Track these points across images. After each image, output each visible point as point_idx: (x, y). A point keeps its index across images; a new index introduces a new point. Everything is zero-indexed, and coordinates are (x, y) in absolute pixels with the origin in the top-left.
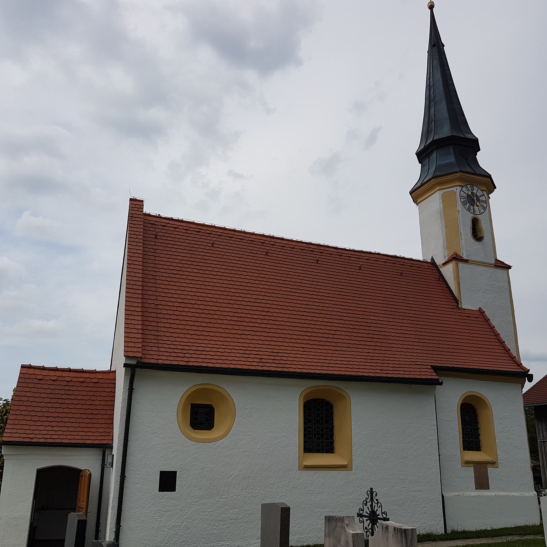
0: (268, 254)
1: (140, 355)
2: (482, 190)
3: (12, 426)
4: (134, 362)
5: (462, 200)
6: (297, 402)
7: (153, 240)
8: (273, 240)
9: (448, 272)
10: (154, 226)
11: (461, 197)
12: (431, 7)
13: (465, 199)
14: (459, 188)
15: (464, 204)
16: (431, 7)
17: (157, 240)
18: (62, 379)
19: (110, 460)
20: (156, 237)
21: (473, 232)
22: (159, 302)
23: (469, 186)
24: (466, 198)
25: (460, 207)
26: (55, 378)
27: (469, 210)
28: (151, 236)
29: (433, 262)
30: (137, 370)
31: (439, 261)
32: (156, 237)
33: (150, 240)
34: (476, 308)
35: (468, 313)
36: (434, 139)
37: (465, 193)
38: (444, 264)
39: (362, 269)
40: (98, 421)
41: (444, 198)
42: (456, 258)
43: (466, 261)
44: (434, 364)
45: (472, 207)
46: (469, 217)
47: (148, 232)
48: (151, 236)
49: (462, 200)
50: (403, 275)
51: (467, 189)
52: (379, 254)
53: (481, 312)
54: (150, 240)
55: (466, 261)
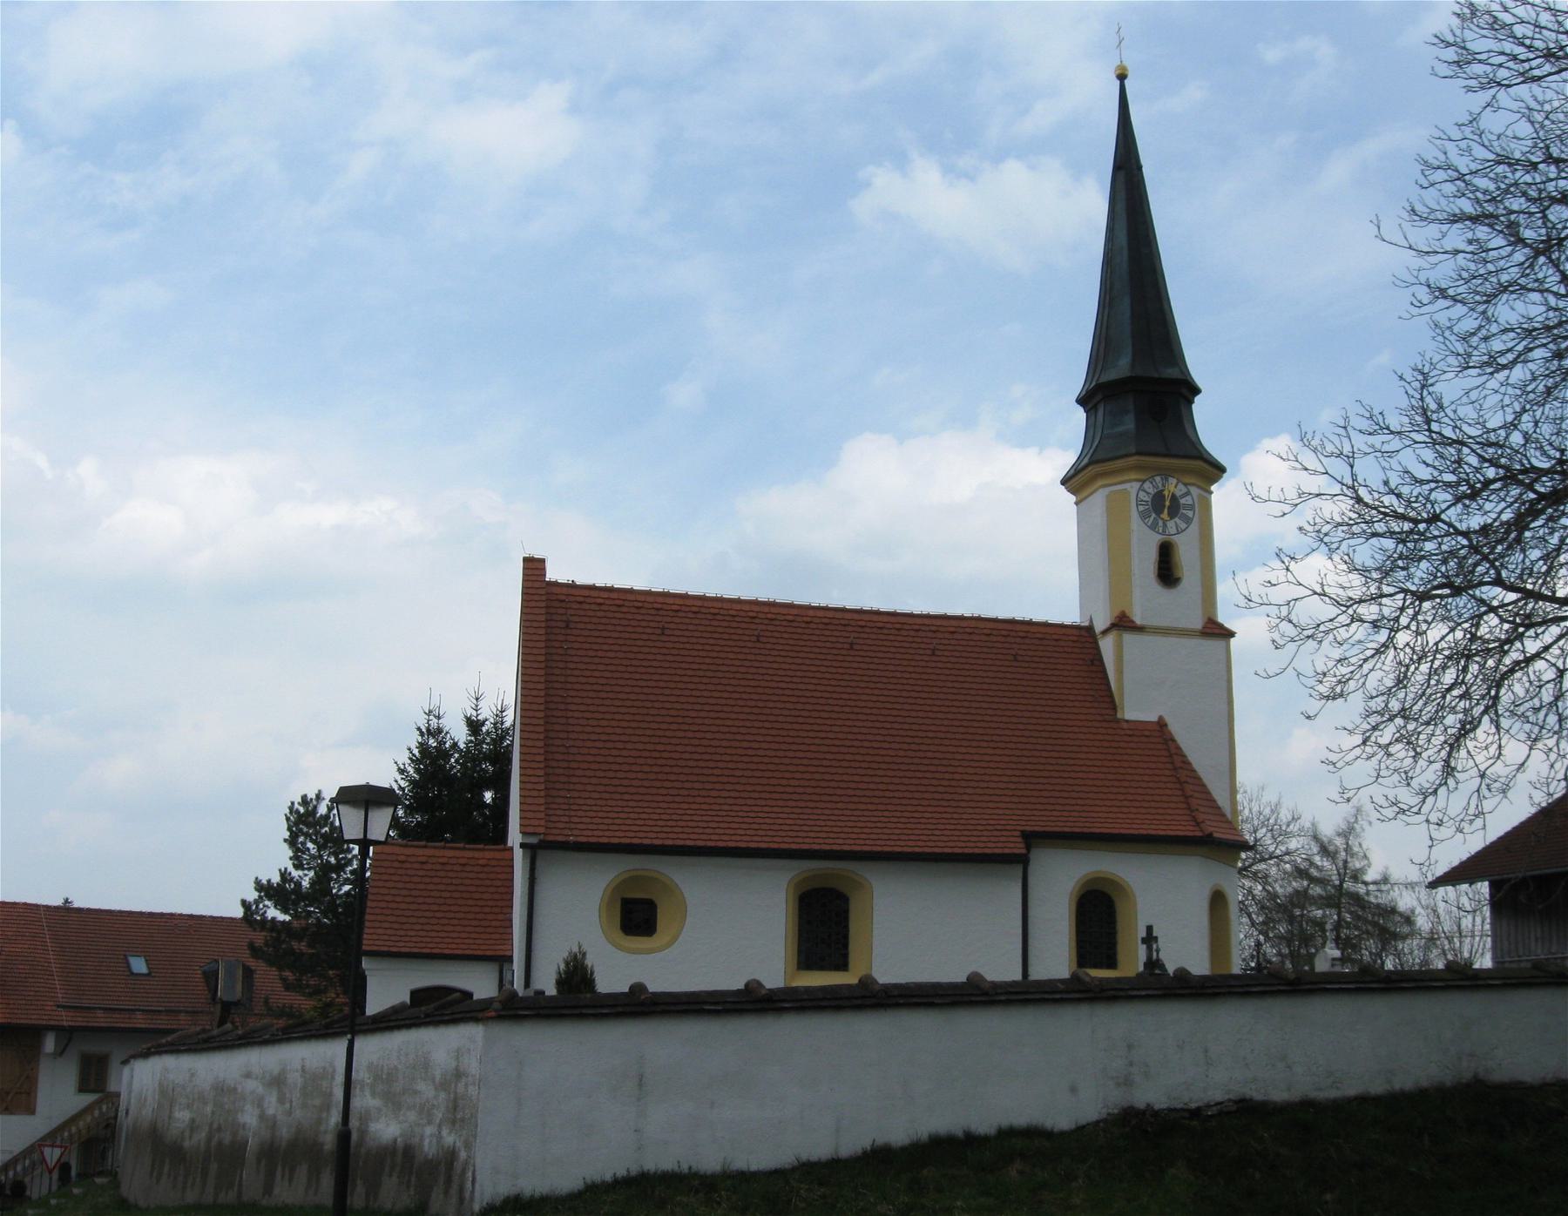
0: (761, 639)
1: (542, 830)
2: (1186, 485)
3: (372, 931)
4: (533, 840)
5: (1141, 508)
6: (783, 895)
7: (563, 631)
8: (773, 610)
9: (1107, 646)
10: (563, 605)
11: (1139, 502)
12: (1122, 77)
14: (1136, 485)
15: (1144, 516)
16: (1122, 77)
17: (569, 631)
18: (434, 860)
19: (509, 977)
20: (567, 627)
21: (1160, 568)
22: (571, 743)
23: (1158, 479)
25: (1136, 522)
26: (424, 859)
27: (1153, 527)
28: (560, 624)
29: (1089, 629)
30: (540, 853)
31: (1099, 626)
32: (567, 627)
33: (558, 631)
34: (1154, 718)
35: (1139, 728)
36: (1101, 381)
38: (1105, 632)
39: (937, 653)
40: (1126, 1082)
41: (1110, 500)
42: (1123, 623)
43: (1140, 629)
44: (1028, 828)
46: (1155, 539)
47: (554, 617)
48: (560, 624)
49: (1141, 508)
50: (1020, 658)
52: (979, 619)
53: (1161, 724)
54: (558, 631)
55: (1140, 629)
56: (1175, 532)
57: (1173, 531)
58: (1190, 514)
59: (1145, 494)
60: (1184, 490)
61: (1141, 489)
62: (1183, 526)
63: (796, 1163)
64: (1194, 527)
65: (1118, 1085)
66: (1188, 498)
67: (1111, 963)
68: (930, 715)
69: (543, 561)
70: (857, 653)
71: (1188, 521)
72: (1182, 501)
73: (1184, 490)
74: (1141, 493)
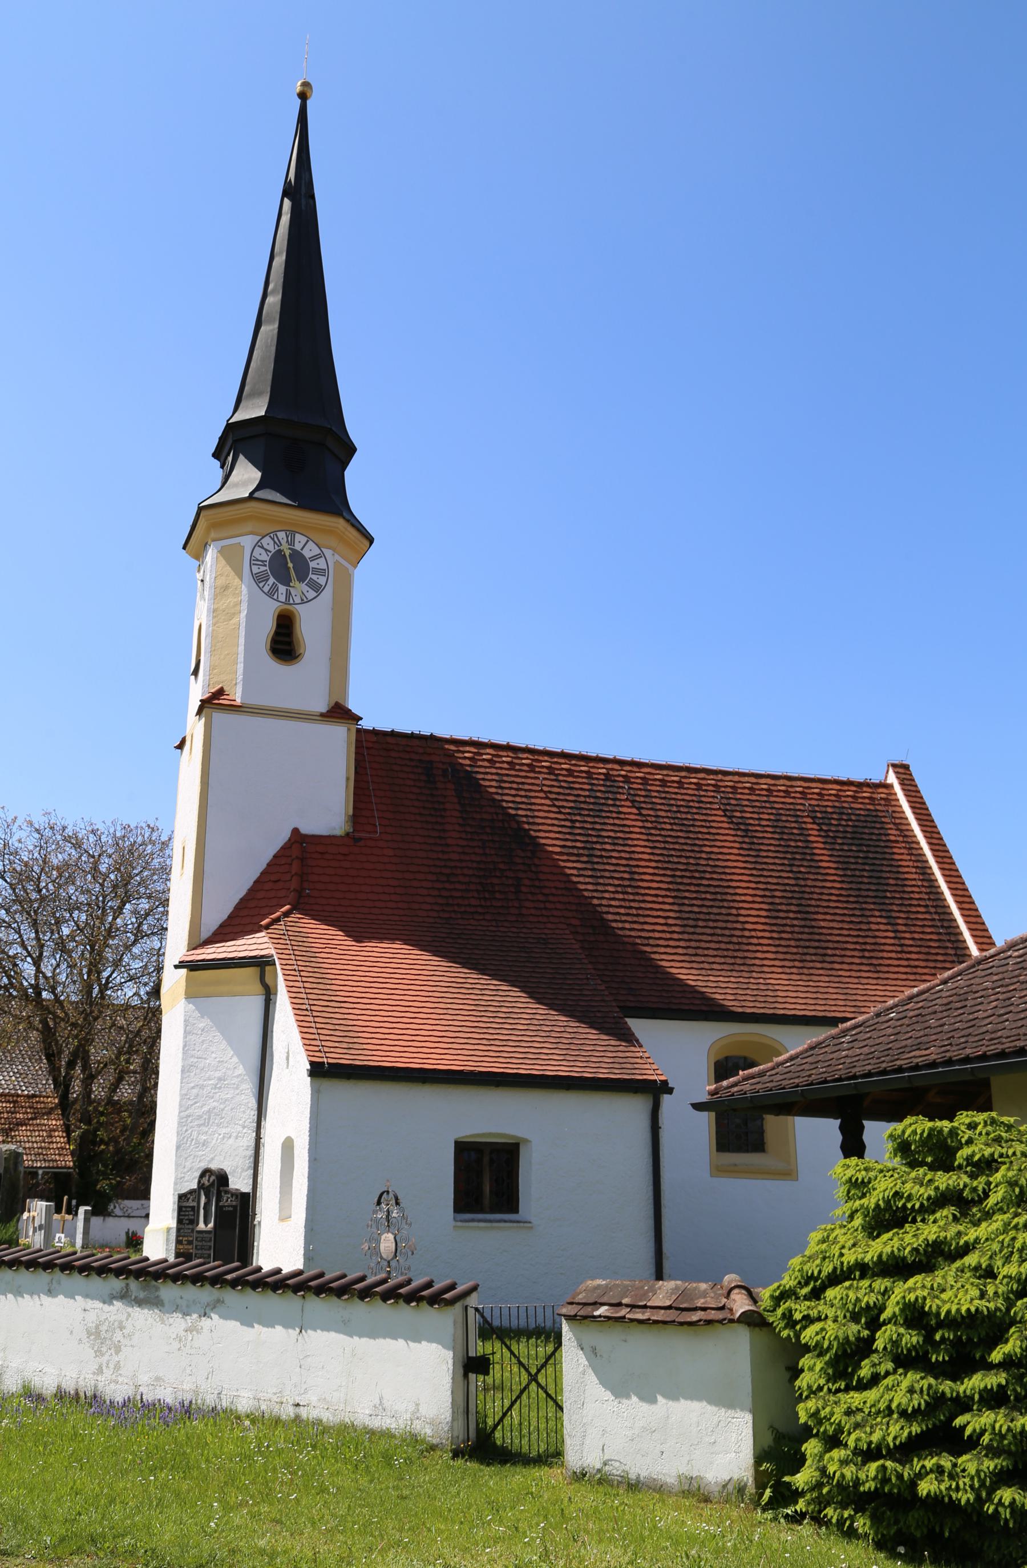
5: (255, 569)
11: (253, 561)
12: (303, 96)
13: (265, 566)
16: (303, 96)
24: (267, 564)
27: (272, 593)
37: (266, 550)
45: (282, 589)
46: (269, 611)
51: (275, 542)
56: (300, 601)
57: (298, 600)
58: (322, 580)
59: (263, 551)
60: (317, 551)
61: (258, 545)
62: (311, 594)
63: (288, 1412)
64: (327, 594)
65: (223, 1302)
66: (322, 561)
67: (993, 944)
68: (671, 943)
69: (462, 1149)
70: (685, 791)
71: (318, 589)
72: (312, 564)
73: (317, 551)
74: (258, 550)
